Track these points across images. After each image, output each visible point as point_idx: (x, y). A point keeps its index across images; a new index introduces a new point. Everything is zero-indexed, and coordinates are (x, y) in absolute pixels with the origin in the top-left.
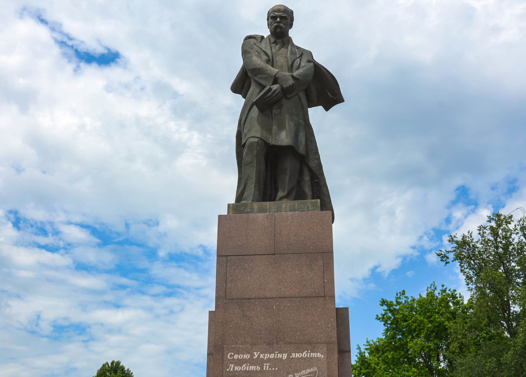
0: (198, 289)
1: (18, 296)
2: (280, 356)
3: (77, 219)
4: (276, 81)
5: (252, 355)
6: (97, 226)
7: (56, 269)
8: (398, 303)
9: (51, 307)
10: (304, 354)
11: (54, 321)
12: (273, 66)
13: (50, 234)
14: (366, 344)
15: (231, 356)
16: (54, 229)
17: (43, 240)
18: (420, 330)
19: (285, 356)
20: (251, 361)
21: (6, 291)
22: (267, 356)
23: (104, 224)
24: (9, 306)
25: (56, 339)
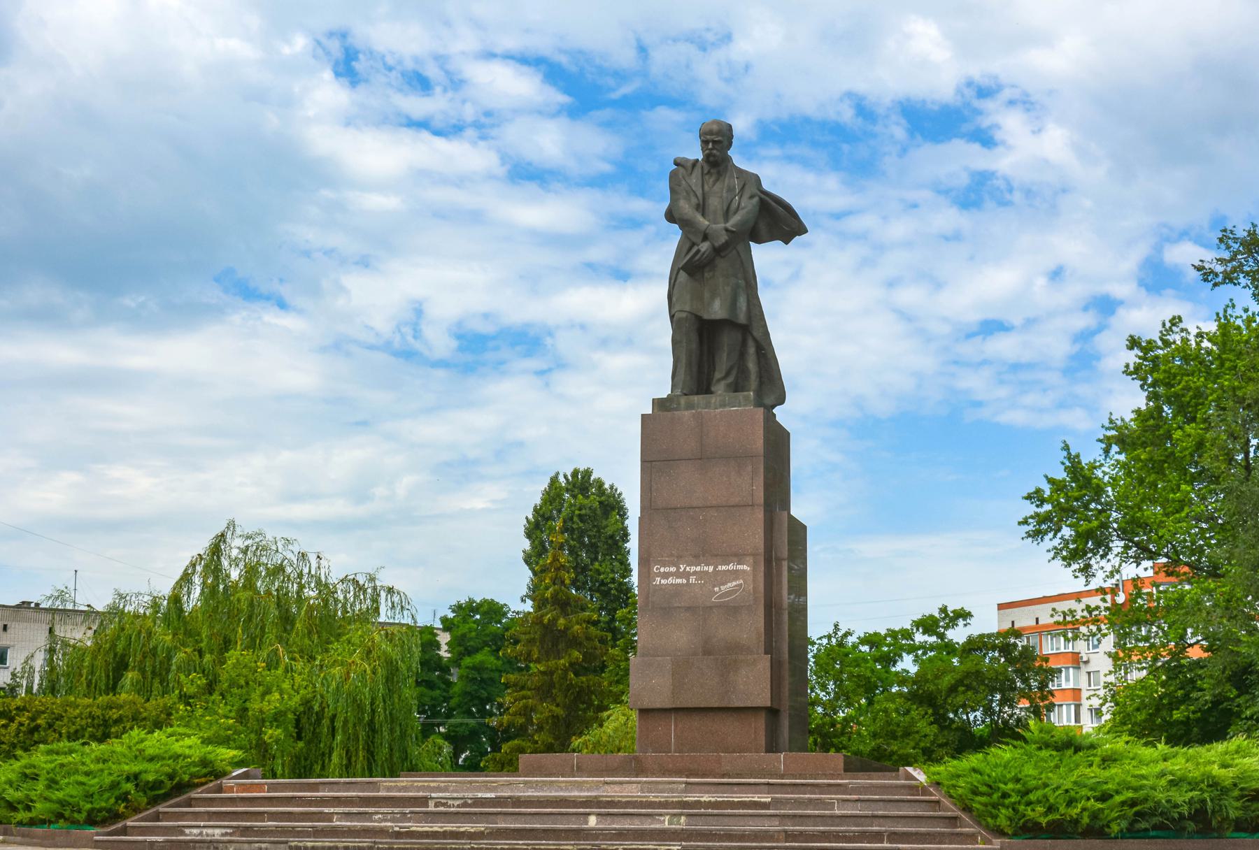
0: (838, 216)
1: (364, 263)
2: (706, 568)
3: (510, 42)
4: (705, 237)
6: (563, 59)
7: (460, 181)
8: (1167, 344)
9: (451, 286)
10: (731, 567)
11: (460, 324)
12: (703, 215)
13: (438, 90)
14: (1107, 424)
16: (447, 72)
17: (417, 105)
18: (1197, 405)
19: (711, 569)
20: (678, 575)
21: (332, 250)
22: (693, 569)
23: (580, 52)
24: (342, 289)
25: (468, 369)
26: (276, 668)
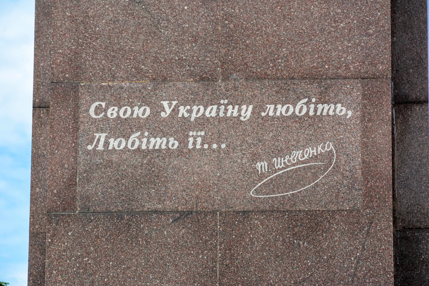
5: (157, 110)
10: (300, 108)
15: (98, 110)
19: (247, 112)
20: (155, 126)
22: (197, 111)
26: (325, 148)
